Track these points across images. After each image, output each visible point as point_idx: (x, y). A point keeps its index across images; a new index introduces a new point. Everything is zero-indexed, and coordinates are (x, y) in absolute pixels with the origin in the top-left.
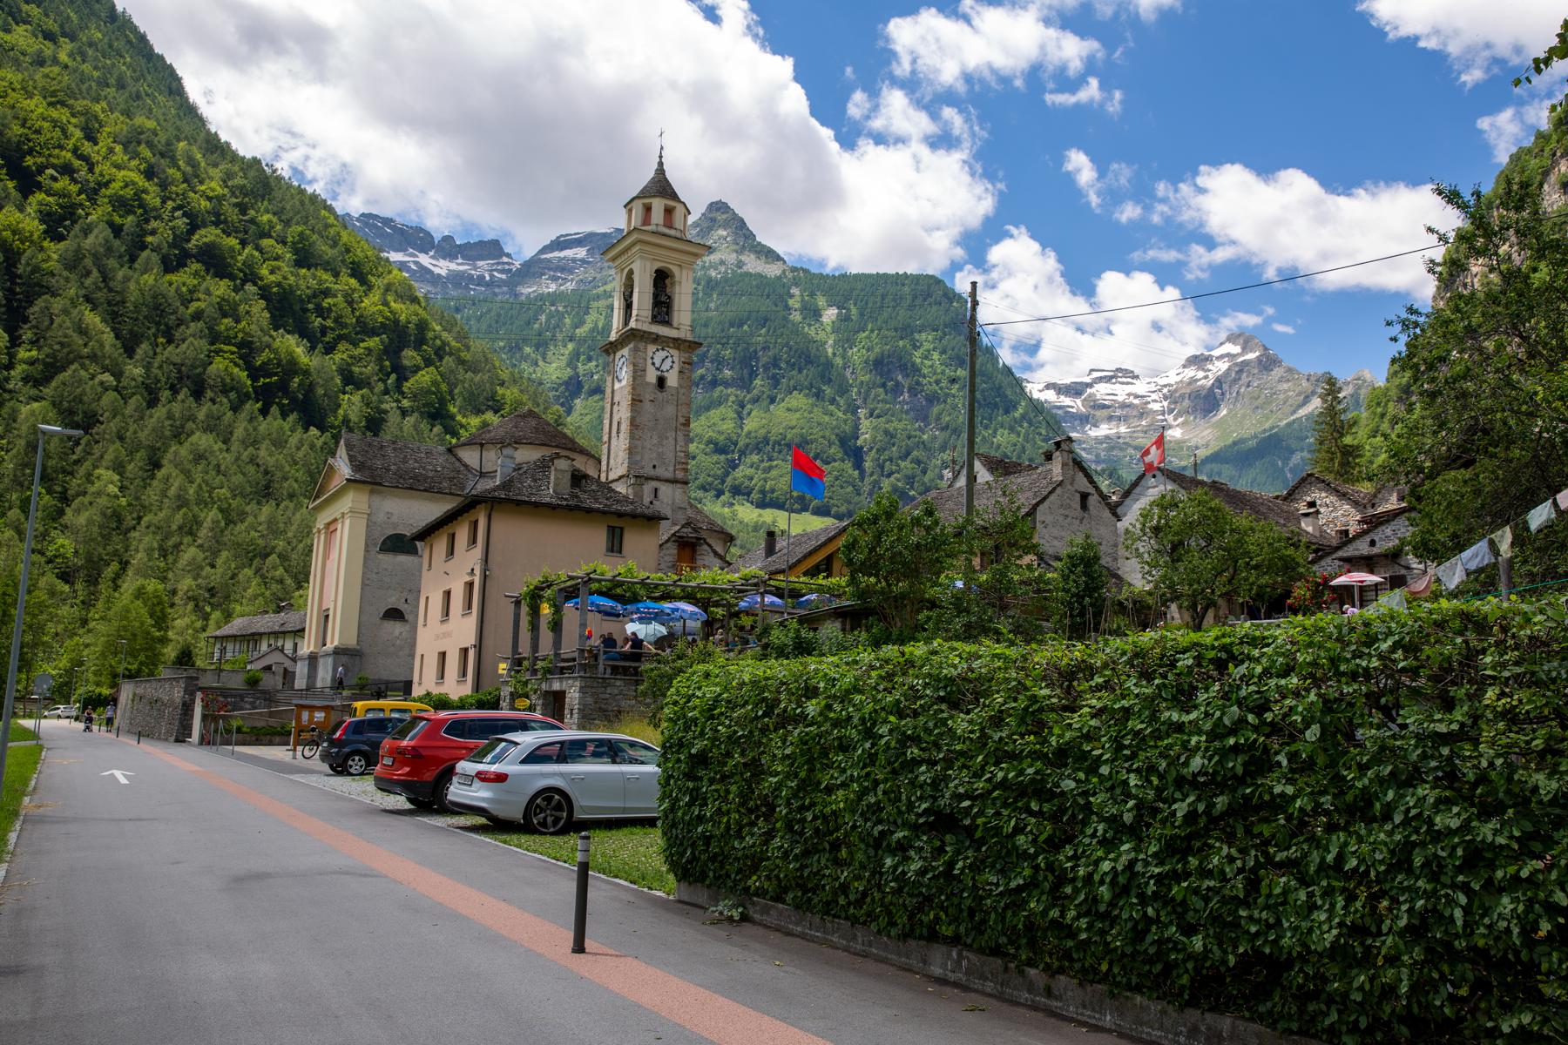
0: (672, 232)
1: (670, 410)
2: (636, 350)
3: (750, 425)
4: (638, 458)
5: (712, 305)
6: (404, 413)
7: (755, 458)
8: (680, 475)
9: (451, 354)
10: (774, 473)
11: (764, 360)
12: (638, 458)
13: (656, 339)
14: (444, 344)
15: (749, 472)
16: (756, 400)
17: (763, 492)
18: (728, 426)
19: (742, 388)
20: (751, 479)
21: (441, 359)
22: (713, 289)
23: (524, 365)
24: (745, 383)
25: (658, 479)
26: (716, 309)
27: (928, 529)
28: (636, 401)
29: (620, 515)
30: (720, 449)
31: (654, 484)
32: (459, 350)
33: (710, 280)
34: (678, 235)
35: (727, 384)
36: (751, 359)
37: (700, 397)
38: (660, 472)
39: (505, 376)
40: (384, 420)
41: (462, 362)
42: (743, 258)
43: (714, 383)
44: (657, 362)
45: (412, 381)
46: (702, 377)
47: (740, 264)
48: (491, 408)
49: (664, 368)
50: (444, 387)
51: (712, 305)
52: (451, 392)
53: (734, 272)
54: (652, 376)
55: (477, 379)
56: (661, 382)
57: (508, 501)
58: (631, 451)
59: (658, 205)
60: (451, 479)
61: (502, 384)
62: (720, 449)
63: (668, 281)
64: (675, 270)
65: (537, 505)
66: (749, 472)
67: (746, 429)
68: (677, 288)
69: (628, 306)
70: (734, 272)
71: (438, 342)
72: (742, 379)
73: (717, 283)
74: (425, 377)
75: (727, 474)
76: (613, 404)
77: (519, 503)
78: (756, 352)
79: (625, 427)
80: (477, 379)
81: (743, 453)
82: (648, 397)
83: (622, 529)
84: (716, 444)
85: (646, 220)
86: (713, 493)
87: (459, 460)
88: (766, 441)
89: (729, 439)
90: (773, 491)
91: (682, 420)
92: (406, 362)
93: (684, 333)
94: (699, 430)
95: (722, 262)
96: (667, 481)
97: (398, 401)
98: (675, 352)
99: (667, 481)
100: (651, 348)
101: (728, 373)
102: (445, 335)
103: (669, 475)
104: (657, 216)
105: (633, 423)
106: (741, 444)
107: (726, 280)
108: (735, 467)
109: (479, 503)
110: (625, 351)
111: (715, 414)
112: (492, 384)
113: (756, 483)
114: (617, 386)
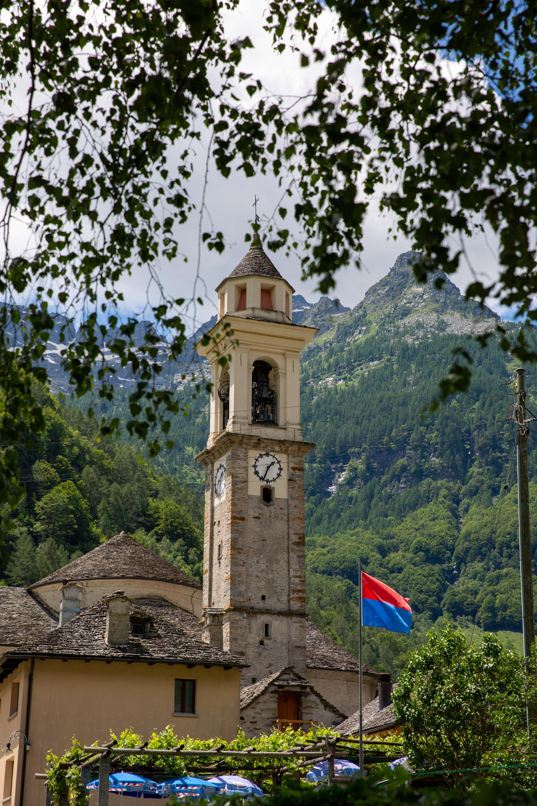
0: (272, 316)
1: (280, 527)
2: (234, 458)
3: (469, 523)
4: (243, 588)
5: (410, 379)
6: (36, 539)
7: (478, 566)
8: (296, 606)
9: (91, 463)
10: (504, 584)
11: (480, 440)
12: (243, 588)
13: (259, 442)
14: (83, 451)
15: (472, 584)
16: (474, 493)
17: (492, 609)
18: (440, 527)
19: (454, 478)
20: (475, 593)
21: (80, 469)
22: (410, 359)
23: (186, 469)
24: (458, 473)
25: (268, 612)
26: (417, 383)
27: (490, 672)
28: (237, 519)
29: (190, 664)
30: (433, 558)
31: (264, 619)
32: (102, 457)
33: (405, 348)
34: (280, 318)
35: (435, 475)
36: (463, 441)
37: (403, 493)
38: (271, 603)
39: (158, 484)
40: (12, 549)
41: (104, 471)
42: (446, 318)
43: (419, 475)
44: (261, 471)
45: (45, 499)
46: (404, 469)
47: (442, 326)
48: (140, 524)
49: (270, 477)
50: (84, 504)
51: (410, 379)
52: (93, 509)
53: (435, 336)
54: (255, 489)
55: (124, 490)
56: (267, 494)
57: (52, 656)
58: (234, 580)
59: (254, 286)
60: (28, 628)
61: (155, 495)
62: (433, 558)
63: (271, 374)
64: (278, 360)
65: (87, 659)
66: (472, 584)
67: (463, 530)
68: (281, 380)
69: (226, 407)
70: (435, 336)
71: (76, 450)
72: (454, 467)
73: (415, 352)
74: (60, 494)
75: (444, 588)
76: (213, 524)
77: (66, 658)
78: (469, 432)
79: (226, 551)
80: (124, 490)
81: (461, 561)
82: (251, 513)
83: (194, 682)
84: (427, 551)
85: (241, 305)
86: (428, 613)
87: (40, 603)
88: (490, 543)
89: (443, 543)
90: (505, 607)
91: (295, 538)
92: (39, 477)
93: (293, 433)
94: (404, 535)
95: (420, 326)
96: (280, 613)
97: (29, 524)
98: (282, 458)
99: (280, 613)
100: (253, 454)
101: (435, 460)
102: (84, 441)
103: (282, 606)
104: (254, 299)
105: (235, 546)
106: (459, 549)
107: (425, 346)
108: (453, 579)
109: (20, 661)
110: (223, 461)
111: (423, 513)
112: (143, 495)
113: (483, 598)
114: (217, 502)
